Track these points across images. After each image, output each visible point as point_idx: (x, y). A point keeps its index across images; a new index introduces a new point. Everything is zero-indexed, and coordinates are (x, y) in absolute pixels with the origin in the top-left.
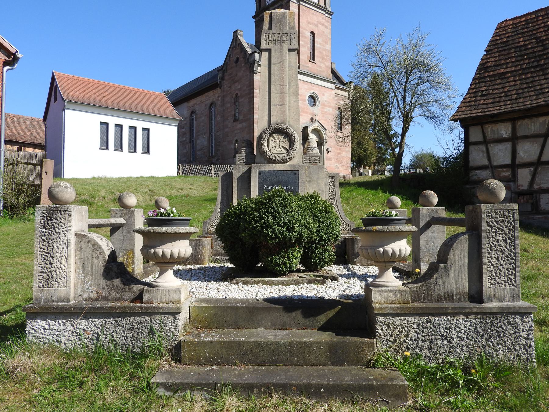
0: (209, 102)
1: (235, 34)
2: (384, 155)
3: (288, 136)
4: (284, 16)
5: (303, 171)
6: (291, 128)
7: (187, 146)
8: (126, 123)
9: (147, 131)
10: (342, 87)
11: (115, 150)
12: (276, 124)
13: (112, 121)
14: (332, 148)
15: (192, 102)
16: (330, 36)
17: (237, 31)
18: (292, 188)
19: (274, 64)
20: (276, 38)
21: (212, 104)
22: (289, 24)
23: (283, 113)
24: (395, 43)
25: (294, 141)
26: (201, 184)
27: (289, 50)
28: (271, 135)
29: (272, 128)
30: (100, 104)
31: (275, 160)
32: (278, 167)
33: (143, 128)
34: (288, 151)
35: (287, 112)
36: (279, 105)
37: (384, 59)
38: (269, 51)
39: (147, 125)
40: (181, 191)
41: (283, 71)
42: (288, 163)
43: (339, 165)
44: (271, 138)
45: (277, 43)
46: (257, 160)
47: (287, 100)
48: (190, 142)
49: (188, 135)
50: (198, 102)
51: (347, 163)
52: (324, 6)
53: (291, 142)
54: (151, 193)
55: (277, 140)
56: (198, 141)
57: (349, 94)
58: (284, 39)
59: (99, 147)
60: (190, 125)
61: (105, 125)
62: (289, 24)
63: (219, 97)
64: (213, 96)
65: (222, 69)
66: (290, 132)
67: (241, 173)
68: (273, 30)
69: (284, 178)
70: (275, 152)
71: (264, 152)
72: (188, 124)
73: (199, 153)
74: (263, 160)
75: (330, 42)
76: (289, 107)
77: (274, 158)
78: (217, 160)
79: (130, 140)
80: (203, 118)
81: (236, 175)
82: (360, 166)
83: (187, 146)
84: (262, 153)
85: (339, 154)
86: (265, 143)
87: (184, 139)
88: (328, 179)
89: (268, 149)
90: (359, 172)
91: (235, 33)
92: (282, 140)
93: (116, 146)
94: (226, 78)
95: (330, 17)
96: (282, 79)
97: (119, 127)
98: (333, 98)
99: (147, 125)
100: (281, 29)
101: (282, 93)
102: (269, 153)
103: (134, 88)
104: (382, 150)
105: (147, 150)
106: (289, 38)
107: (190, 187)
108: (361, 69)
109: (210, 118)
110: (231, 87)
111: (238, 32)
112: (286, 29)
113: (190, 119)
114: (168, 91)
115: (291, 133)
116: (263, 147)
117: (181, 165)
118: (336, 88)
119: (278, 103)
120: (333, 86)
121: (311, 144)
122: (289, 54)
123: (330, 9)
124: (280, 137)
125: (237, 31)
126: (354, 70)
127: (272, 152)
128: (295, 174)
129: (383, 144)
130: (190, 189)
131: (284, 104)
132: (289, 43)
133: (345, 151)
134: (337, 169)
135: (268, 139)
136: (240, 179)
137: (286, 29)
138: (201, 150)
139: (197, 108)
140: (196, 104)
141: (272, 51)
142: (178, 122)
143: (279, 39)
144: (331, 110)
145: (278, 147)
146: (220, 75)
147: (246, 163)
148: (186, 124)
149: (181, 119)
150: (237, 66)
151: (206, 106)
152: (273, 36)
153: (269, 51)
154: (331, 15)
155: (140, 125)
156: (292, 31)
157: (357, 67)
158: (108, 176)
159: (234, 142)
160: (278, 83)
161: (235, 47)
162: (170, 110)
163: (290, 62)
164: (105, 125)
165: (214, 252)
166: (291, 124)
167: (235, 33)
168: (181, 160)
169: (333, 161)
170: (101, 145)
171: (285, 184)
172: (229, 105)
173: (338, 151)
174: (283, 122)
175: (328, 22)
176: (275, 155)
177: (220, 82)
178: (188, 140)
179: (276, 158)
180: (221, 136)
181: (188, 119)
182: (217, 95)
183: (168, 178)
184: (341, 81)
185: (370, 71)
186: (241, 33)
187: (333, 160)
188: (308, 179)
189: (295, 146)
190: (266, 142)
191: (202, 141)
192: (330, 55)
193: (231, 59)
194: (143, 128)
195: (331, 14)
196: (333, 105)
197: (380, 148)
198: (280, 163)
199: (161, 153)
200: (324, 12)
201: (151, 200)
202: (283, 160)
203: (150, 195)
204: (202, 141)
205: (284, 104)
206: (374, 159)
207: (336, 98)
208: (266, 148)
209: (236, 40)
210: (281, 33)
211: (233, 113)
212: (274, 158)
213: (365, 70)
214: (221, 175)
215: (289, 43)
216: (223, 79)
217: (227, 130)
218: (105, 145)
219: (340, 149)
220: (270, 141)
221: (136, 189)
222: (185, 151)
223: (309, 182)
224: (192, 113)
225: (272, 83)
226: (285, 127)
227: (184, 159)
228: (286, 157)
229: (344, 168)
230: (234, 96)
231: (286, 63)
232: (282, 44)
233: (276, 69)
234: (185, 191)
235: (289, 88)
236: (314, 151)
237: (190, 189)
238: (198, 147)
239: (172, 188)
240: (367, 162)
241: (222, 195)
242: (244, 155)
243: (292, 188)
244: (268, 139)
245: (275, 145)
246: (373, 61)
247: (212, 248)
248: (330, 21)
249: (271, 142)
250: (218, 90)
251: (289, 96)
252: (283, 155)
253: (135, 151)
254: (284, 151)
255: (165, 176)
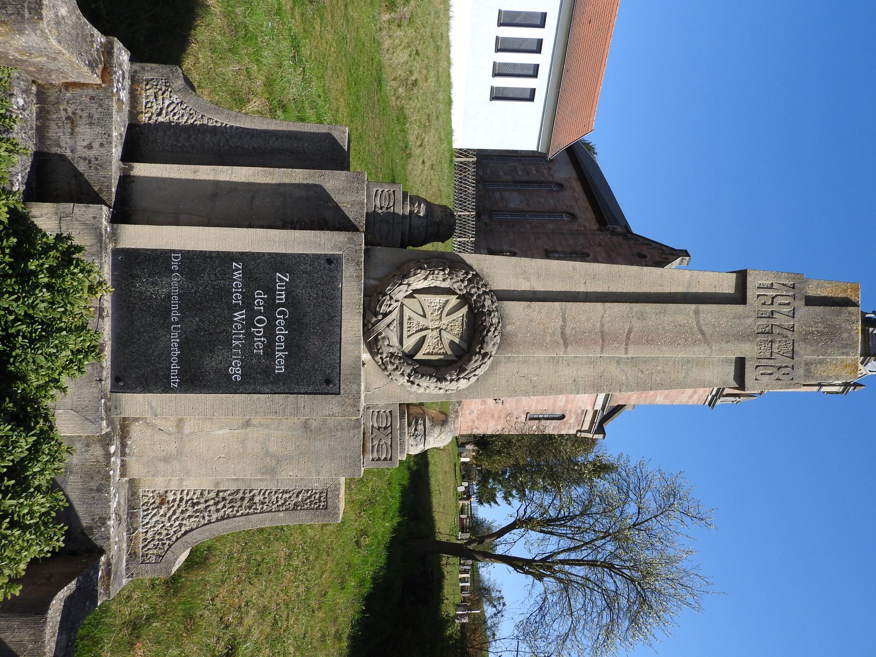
0: (576, 211)
1: (684, 253)
2: (494, 480)
3: (459, 357)
4: (846, 346)
5: (337, 410)
6: (485, 368)
7: (509, 177)
8: (544, 60)
9: (530, 96)
10: (597, 420)
11: (497, 38)
12: (501, 318)
13: (548, 35)
14: (500, 405)
15: (577, 186)
16: (676, 403)
17: (689, 256)
18: (280, 368)
19: (697, 312)
20: (780, 319)
21: (573, 216)
22: (821, 362)
23: (538, 342)
24: (684, 545)
25: (441, 379)
26: (434, 183)
27: (740, 364)
28: (465, 299)
29: (488, 303)
30: (577, 14)
31: (376, 314)
32: (351, 324)
33: (535, 89)
34: (409, 357)
35: (541, 354)
36: (563, 328)
37: (653, 524)
38: (740, 297)
39: (540, 96)
40: (419, 143)
41: (673, 342)
42: (366, 356)
43: (474, 415)
44: (453, 300)
45: (764, 321)
46: (381, 253)
47: (582, 353)
48: (515, 182)
49: (525, 178)
50: (576, 195)
51: (477, 428)
52: (725, 393)
53: (437, 369)
54: (410, 82)
55: (445, 321)
56: (515, 194)
57: (584, 431)
58: (776, 346)
59: (503, 9)
60: (542, 182)
61: (540, 21)
62: (821, 362)
63: (585, 227)
64: (587, 218)
65: (631, 233)
66: (472, 365)
67: (336, 198)
68: (804, 311)
69: (314, 344)
70: (407, 313)
71: (406, 276)
72: (542, 178)
73: (497, 195)
74: (379, 272)
75: (667, 402)
76: (555, 361)
77: (384, 309)
78: (485, 223)
79: (515, 65)
80: (552, 202)
81: (331, 181)
82: (476, 444)
83: (509, 177)
84: (401, 274)
85: (493, 415)
86: (438, 280)
87: (520, 173)
88: (317, 486)
89: (416, 291)
90: (467, 443)
91: (685, 253)
92: (447, 337)
93: (505, 39)
94: (615, 238)
95: (707, 403)
96: (649, 340)
97: (537, 47)
98: (580, 408)
99: (540, 96)
100: (806, 337)
101: (604, 338)
102: (400, 292)
103: (603, 79)
104: (500, 475)
105: (498, 95)
106: (780, 360)
107: (428, 164)
108: (633, 479)
109: (553, 212)
110: (600, 245)
111: (687, 258)
112: (805, 353)
113: (551, 183)
114: (595, 153)
115: (470, 368)
116: (422, 274)
117: (475, 159)
118: (596, 412)
119: (570, 325)
120: (598, 407)
121: (437, 430)
122: (726, 361)
123: (718, 402)
124: (457, 330)
125: (689, 256)
126: (632, 464)
127: (408, 302)
128: (328, 382)
129: (509, 477)
130: (423, 162)
131: (566, 344)
132: (764, 362)
133: (496, 425)
134: (468, 412)
135: (449, 291)
136: (319, 194)
137: (805, 353)
138: (502, 197)
139: (568, 193)
140: (575, 191)
141: (739, 308)
142: (544, 151)
143: (776, 330)
144: (562, 404)
145: (423, 322)
146: (619, 229)
147: (372, 218)
148: (543, 176)
149: (550, 156)
150: (633, 255)
151: (572, 206)
152: (786, 310)
153: (740, 297)
154: (710, 405)
155: (540, 84)
156: (801, 371)
157: (638, 470)
158: (453, 23)
159: (513, 249)
160: (637, 326)
161: (663, 252)
162: (564, 140)
163: (701, 363)
164: (540, 21)
165: (52, 95)
166: (502, 369)
167: (685, 253)
168: (484, 157)
169: (481, 407)
170: (507, 13)
171: (294, 347)
172: (571, 242)
173: (496, 415)
174: (505, 342)
175: (699, 400)
176: (395, 315)
177: (608, 229)
178: (518, 178)
179: (385, 315)
180: (523, 230)
181: (550, 179)
182: (587, 224)
183: (450, 133)
184: (605, 419)
185: (631, 495)
186: (685, 262)
187: (483, 407)
188: (314, 425)
189: (425, 382)
190: (438, 284)
191: (515, 200)
192: (647, 403)
193: (644, 247)
194: (535, 89)
195: (712, 404)
196: (569, 407)
197: (504, 473)
198: (367, 328)
199: (492, 122)
200: (714, 393)
201: (395, 79)
202: (376, 339)
203: (407, 79)
204: (515, 200)
205: (566, 344)
206: (486, 465)
207: (579, 411)
208: (418, 282)
209: (675, 255)
210: (796, 336)
211: (559, 249)
212: (384, 309)
213: (631, 487)
214: (336, 134)
215: (764, 362)
216: (613, 233)
217: (532, 238)
218: (507, 19)
219: (500, 417)
220: (443, 298)
221: (417, 53)
222: (501, 174)
223: (306, 426)
224: (561, 186)
225: (637, 307)
226: (490, 348)
227: (488, 171)
228: (386, 350)
229: (470, 424)
230: (586, 250)
231: (698, 352)
232: (761, 338)
233: (680, 319)
234: (418, 151)
235: (619, 361)
236: (412, 441)
237: (423, 162)
238: (506, 194)
239: (425, 128)
240: (481, 455)
241: (266, 133)
242: (399, 210)
243: (280, 368)
244: (449, 291)
245: (428, 312)
246: (651, 503)
247: (68, 86)
248: (701, 403)
249: (439, 299)
250: (595, 226)
251: (591, 362)
252: (395, 341)
253: (496, 74)
254: (409, 344)
255: (453, 127)
